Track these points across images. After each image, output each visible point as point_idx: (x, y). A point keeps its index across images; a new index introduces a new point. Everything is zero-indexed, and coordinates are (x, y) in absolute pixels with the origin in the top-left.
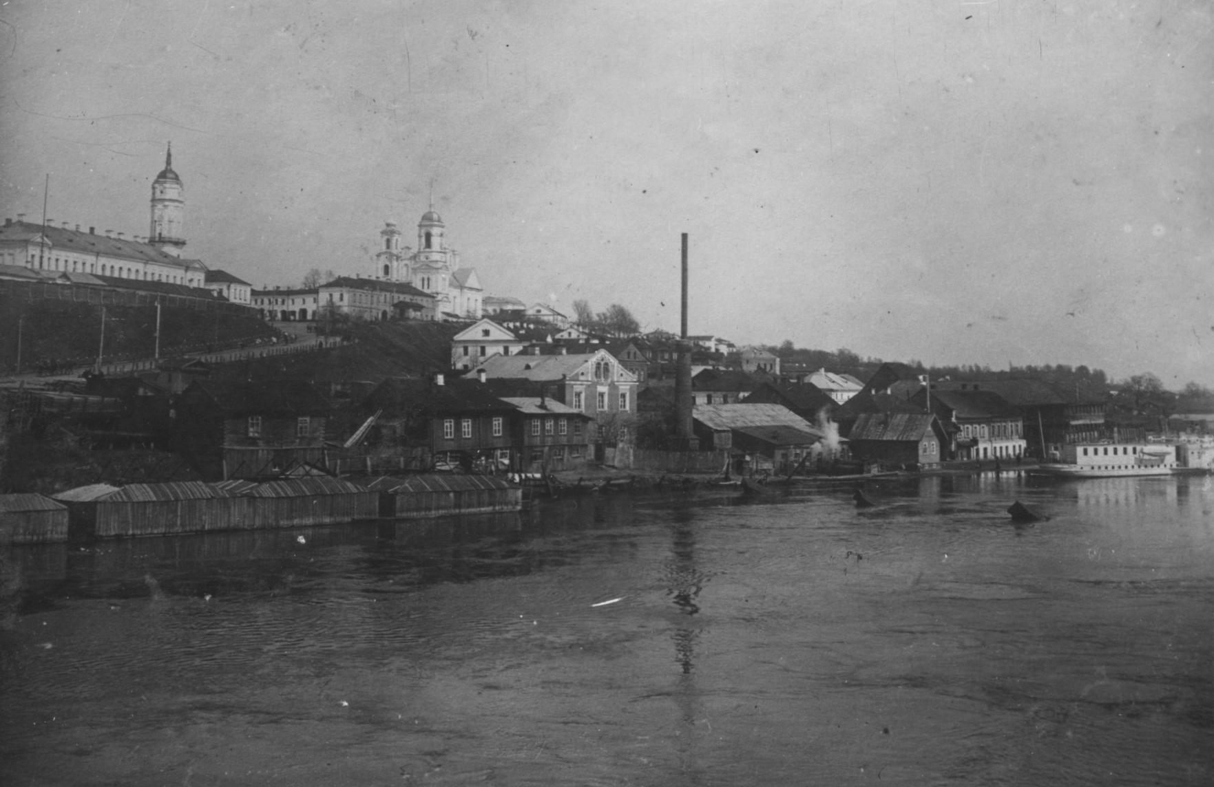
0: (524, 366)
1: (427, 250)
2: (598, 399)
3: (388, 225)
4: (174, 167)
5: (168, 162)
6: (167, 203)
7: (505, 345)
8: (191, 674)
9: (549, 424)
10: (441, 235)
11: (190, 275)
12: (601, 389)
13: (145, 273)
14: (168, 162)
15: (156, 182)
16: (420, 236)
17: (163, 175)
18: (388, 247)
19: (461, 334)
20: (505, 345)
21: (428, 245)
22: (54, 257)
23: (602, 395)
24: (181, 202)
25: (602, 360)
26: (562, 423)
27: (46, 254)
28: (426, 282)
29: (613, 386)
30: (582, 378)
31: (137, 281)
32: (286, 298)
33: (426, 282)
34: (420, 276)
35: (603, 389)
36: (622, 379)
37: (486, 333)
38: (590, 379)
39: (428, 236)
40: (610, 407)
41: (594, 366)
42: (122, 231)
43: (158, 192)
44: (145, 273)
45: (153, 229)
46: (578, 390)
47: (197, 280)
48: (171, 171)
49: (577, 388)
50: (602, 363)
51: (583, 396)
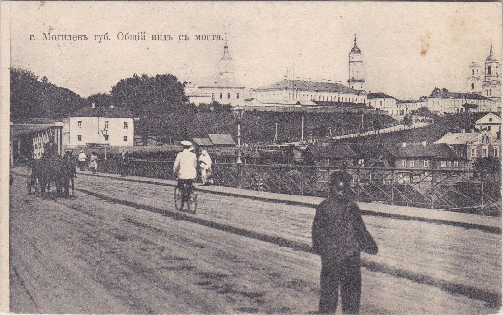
0: (456, 138)
1: (489, 75)
4: (358, 46)
5: (355, 44)
6: (355, 63)
8: (64, 189)
9: (449, 163)
10: (497, 67)
11: (360, 97)
12: (484, 147)
13: (339, 98)
14: (355, 44)
15: (350, 53)
16: (485, 69)
17: (353, 50)
18: (473, 74)
24: (362, 62)
26: (456, 163)
27: (295, 93)
30: (474, 143)
31: (327, 102)
32: (413, 104)
37: (491, 120)
38: (479, 143)
39: (490, 68)
43: (351, 58)
45: (14, 178)
46: (496, 149)
47: (361, 99)
48: (357, 48)
49: (473, 148)
50: (485, 136)
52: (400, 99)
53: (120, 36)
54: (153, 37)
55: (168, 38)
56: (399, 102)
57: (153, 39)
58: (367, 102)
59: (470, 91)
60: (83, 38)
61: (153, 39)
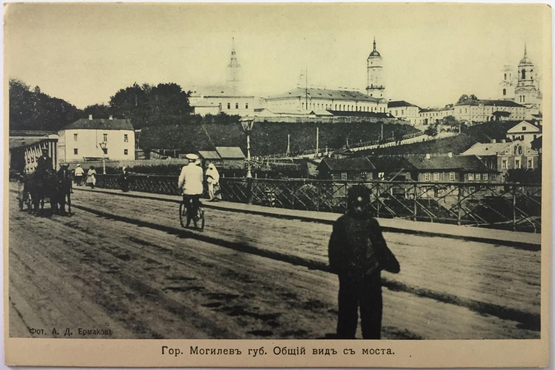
2: (528, 165)
3: (505, 66)
4: (377, 50)
7: (535, 134)
9: (478, 176)
10: (532, 71)
12: (517, 158)
13: (357, 107)
14: (374, 48)
17: (372, 54)
18: (505, 79)
19: (511, 129)
20: (535, 134)
21: (524, 77)
22: (312, 103)
23: (517, 161)
25: (518, 145)
26: (344, 174)
28: (522, 98)
29: (524, 158)
30: (506, 154)
33: (522, 98)
34: (519, 94)
35: (519, 158)
36: (530, 154)
37: (524, 128)
40: (522, 166)
41: (514, 148)
42: (245, 105)
44: (357, 107)
48: (376, 52)
50: (518, 146)
51: (532, 162)
52: (423, 108)
53: (277, 351)
54: (314, 352)
55: (331, 352)
56: (422, 111)
57: (314, 353)
58: (388, 110)
59: (501, 97)
60: (236, 352)
61: (314, 353)
